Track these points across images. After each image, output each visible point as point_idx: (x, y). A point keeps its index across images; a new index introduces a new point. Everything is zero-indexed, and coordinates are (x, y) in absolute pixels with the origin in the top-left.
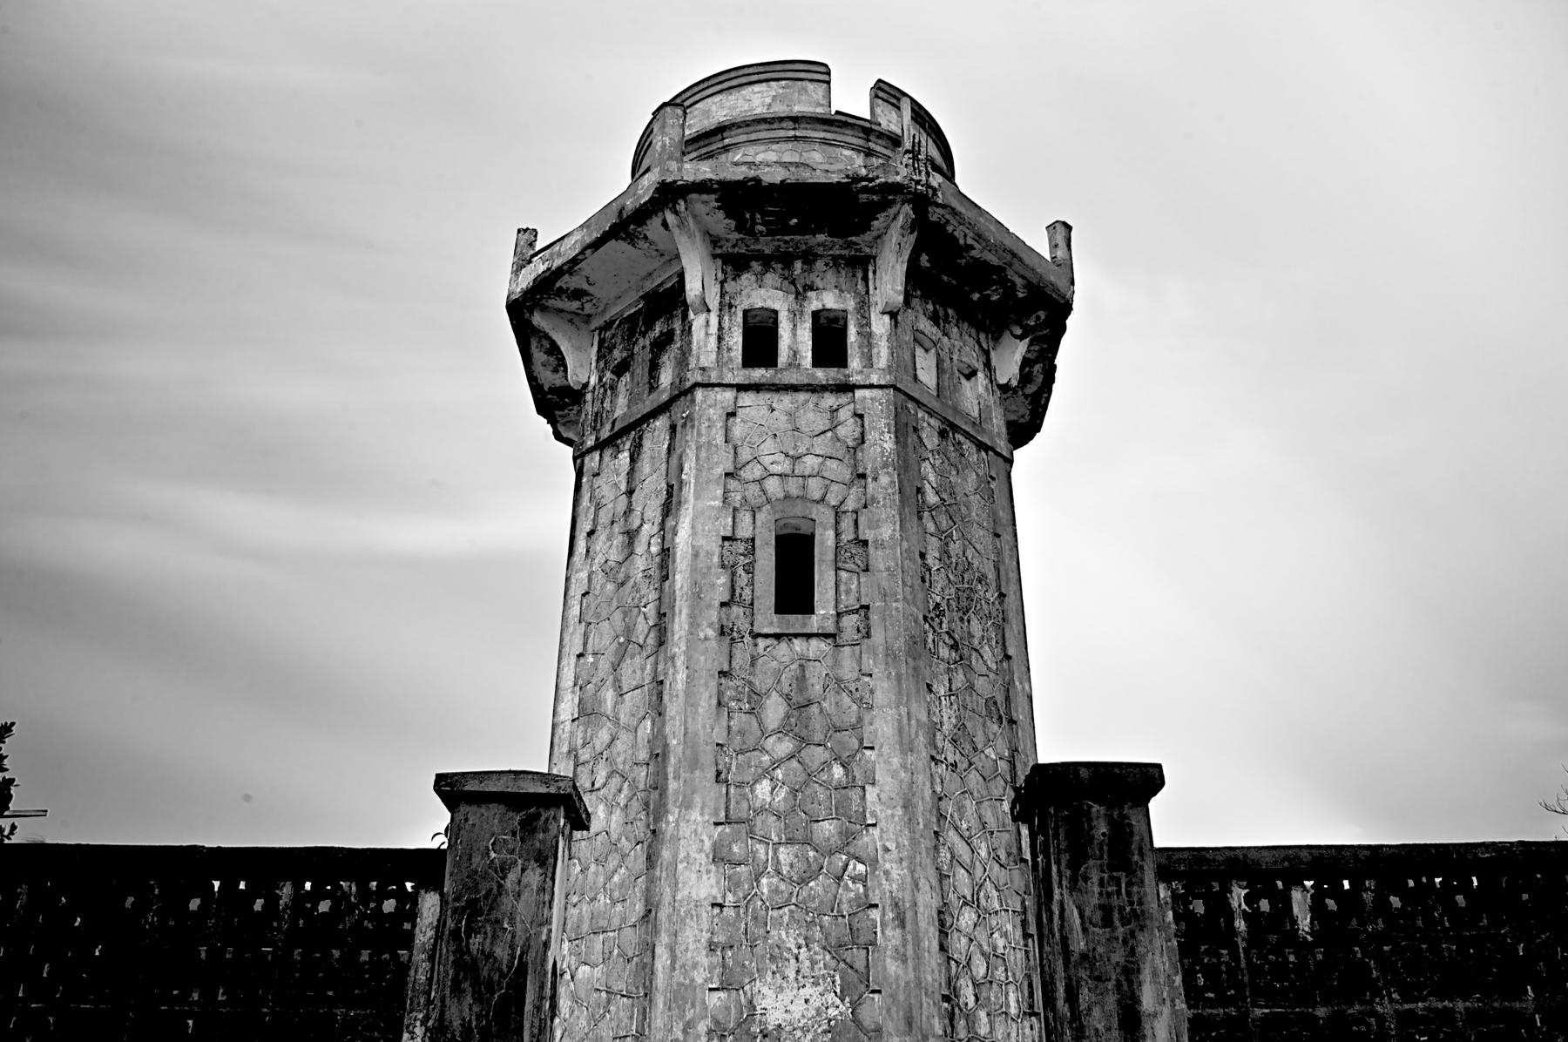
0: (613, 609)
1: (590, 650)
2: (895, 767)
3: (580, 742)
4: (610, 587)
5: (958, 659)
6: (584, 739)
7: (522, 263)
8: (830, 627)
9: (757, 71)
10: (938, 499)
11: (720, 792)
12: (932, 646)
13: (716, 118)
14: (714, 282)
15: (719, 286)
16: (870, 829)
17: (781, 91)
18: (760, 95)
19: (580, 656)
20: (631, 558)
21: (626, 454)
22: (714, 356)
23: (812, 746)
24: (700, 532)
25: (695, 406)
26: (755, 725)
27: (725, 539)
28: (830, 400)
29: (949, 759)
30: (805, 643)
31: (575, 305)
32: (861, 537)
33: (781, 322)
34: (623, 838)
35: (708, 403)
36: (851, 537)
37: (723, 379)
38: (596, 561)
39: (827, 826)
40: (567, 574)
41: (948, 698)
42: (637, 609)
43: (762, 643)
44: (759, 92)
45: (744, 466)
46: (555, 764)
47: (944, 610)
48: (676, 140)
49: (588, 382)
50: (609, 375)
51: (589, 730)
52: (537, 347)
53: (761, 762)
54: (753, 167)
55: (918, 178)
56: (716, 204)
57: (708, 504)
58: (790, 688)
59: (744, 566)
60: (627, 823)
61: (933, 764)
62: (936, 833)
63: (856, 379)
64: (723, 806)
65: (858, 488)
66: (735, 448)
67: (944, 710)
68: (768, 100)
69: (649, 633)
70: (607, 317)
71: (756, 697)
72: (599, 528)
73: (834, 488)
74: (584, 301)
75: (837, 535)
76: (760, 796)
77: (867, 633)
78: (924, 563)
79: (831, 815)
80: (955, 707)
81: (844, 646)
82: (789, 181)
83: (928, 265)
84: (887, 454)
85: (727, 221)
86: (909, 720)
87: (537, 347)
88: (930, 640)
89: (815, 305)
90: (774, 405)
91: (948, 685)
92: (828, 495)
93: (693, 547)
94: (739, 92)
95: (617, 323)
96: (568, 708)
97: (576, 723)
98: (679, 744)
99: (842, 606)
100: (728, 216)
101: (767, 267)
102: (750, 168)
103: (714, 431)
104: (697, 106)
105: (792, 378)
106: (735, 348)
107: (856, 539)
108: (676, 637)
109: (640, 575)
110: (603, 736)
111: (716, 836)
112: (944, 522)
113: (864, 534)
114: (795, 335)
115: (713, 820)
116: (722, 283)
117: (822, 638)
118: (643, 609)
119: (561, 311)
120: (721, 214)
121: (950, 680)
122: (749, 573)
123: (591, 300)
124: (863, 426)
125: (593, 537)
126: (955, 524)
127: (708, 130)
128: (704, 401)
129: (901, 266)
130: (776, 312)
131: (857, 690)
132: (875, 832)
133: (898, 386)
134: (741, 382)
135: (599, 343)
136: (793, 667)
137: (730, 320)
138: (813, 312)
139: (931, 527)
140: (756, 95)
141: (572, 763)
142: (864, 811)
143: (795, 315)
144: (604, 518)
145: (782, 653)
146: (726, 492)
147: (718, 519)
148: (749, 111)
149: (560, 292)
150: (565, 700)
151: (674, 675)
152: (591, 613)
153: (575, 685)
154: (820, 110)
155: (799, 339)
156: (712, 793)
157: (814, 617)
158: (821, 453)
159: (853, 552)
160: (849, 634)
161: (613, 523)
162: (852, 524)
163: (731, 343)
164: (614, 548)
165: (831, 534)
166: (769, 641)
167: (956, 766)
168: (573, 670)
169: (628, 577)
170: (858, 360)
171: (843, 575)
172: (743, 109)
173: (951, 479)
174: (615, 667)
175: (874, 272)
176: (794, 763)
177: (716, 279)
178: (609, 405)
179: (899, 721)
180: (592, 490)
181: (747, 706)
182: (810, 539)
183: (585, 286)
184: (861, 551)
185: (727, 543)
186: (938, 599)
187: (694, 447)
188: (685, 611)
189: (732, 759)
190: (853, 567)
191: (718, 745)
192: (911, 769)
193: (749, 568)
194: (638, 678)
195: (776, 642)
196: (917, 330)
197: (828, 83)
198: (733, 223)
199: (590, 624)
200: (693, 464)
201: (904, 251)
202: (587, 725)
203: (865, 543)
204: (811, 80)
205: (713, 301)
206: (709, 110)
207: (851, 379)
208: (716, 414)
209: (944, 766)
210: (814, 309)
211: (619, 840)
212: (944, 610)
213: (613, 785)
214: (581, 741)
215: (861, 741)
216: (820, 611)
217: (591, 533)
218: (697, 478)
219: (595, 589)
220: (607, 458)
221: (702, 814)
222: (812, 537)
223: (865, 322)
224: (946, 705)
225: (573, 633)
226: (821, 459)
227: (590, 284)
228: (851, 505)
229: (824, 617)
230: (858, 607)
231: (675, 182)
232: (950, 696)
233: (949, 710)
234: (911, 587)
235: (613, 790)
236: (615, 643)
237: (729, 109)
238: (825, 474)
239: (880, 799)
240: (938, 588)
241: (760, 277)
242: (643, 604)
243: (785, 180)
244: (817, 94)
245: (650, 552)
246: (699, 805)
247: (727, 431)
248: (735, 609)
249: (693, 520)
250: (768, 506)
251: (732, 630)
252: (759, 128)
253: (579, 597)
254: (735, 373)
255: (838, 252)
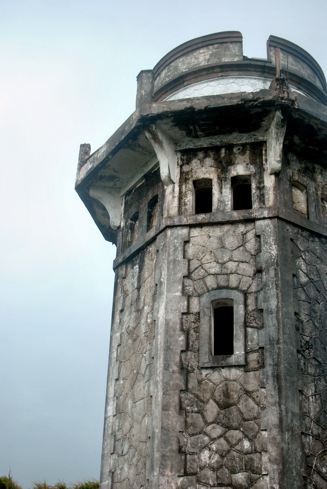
0: (131, 354)
1: (121, 377)
2: (278, 441)
3: (117, 428)
4: (130, 341)
5: (321, 372)
6: (119, 426)
7: (82, 163)
8: (242, 362)
9: (201, 41)
10: (308, 279)
11: (181, 459)
12: (303, 367)
13: (181, 70)
14: (176, 166)
15: (179, 169)
16: (265, 478)
17: (214, 51)
18: (203, 54)
19: (117, 380)
20: (139, 325)
21: (137, 266)
22: (177, 209)
23: (232, 431)
24: (169, 310)
25: (167, 239)
26: (201, 419)
27: (183, 314)
28: (242, 228)
29: (314, 433)
30: (228, 371)
31: (111, 184)
32: (259, 308)
33: (214, 186)
34: (135, 483)
35: (174, 236)
36: (254, 308)
37: (181, 222)
38: (124, 327)
39: (241, 476)
40: (111, 334)
41: (314, 397)
42: (142, 354)
43: (204, 372)
44: (203, 53)
45: (194, 271)
46: (106, 440)
47: (312, 345)
48: (148, 91)
49: (120, 226)
50: (130, 221)
51: (121, 422)
52: (97, 207)
53: (204, 441)
54: (190, 101)
55: (283, 96)
56: (172, 124)
57: (174, 294)
58: (220, 398)
59: (194, 328)
60: (137, 475)
61: (303, 436)
62: (304, 477)
63: (256, 214)
64: (183, 466)
65: (258, 279)
66: (189, 261)
67: (311, 404)
68: (208, 57)
69: (146, 369)
70: (128, 188)
71: (201, 404)
72: (125, 308)
73: (245, 279)
74: (115, 181)
75: (246, 306)
76: (203, 460)
77: (263, 364)
78: (298, 319)
79: (243, 470)
80: (319, 401)
81: (250, 371)
82: (210, 107)
83: (300, 141)
84: (274, 257)
85: (180, 132)
86: (287, 413)
87: (97, 207)
88: (302, 364)
89: (233, 173)
90: (210, 234)
91: (314, 389)
92: (241, 284)
93: (166, 320)
94: (192, 54)
95: (133, 191)
96: (111, 410)
97: (115, 417)
98: (159, 432)
99: (249, 348)
100: (181, 129)
101: (206, 156)
102: (188, 102)
103: (177, 252)
104: (171, 64)
105: (219, 218)
106: (189, 203)
107: (256, 309)
108: (158, 371)
109: (143, 335)
110: (127, 425)
111: (179, 483)
112: (312, 293)
113: (261, 305)
114: (221, 193)
115: (177, 474)
116: (181, 167)
117: (238, 368)
118: (144, 355)
119: (105, 187)
120: (177, 129)
121: (315, 386)
122: (197, 333)
123: (119, 180)
124: (260, 242)
125: (123, 313)
126: (320, 293)
127: (175, 78)
128: (171, 236)
129: (279, 146)
130: (210, 181)
131: (257, 396)
132: (267, 478)
133: (280, 216)
134: (191, 223)
135: (125, 203)
136: (221, 385)
137: (186, 187)
138: (232, 178)
139: (303, 297)
140: (201, 55)
141: (113, 440)
142: (261, 467)
143: (221, 180)
144: (128, 302)
145: (215, 378)
146: (184, 287)
147: (179, 303)
148: (198, 64)
149: (101, 178)
150: (110, 405)
151: (157, 393)
152: (122, 356)
153: (114, 396)
154: (236, 59)
155: (224, 194)
156: (177, 460)
157: (233, 356)
158: (237, 259)
159: (255, 316)
160: (253, 365)
161: (131, 305)
162: (254, 300)
163: (186, 201)
164: (132, 319)
165: (242, 307)
166: (207, 372)
167: (319, 436)
168: (113, 388)
169: (138, 336)
170: (257, 203)
171: (249, 330)
172: (194, 64)
173: (317, 266)
174: (132, 386)
175: (266, 150)
176: (222, 440)
177: (178, 164)
178: (130, 238)
179: (280, 414)
180: (123, 287)
181: (196, 409)
182: (231, 309)
183: (114, 173)
184: (259, 316)
185: (184, 316)
186: (308, 339)
187: (166, 261)
188: (162, 357)
189: (188, 439)
190: (255, 325)
191: (180, 432)
192: (288, 442)
193: (197, 330)
194: (142, 394)
195: (212, 372)
196: (294, 181)
197: (241, 42)
198: (184, 133)
199: (121, 362)
200: (166, 272)
201: (280, 138)
202: (120, 418)
203: (262, 310)
204: (231, 42)
205: (176, 177)
206: (178, 66)
207: (253, 215)
208: (178, 243)
209: (311, 437)
210: (232, 176)
211: (133, 484)
212: (312, 345)
213: (131, 453)
214: (117, 428)
215: (259, 426)
216: (236, 352)
217: (122, 311)
218: (168, 280)
219: (123, 342)
220: (129, 268)
221: (171, 471)
222: (232, 308)
223: (261, 181)
224: (312, 401)
225: (113, 367)
226: (237, 263)
227: (116, 172)
228: (254, 288)
229: (238, 357)
230: (258, 348)
231: (148, 115)
232: (315, 395)
233: (314, 404)
234: (288, 334)
235: (131, 456)
236: (132, 374)
237: (188, 64)
238: (239, 272)
239: (270, 460)
240: (307, 332)
241: (202, 161)
242: (144, 352)
243: (207, 107)
244: (234, 49)
245: (147, 322)
246: (170, 467)
247: (184, 252)
248: (189, 353)
249: (166, 305)
250: (207, 294)
251: (188, 366)
252: (201, 74)
253: (116, 347)
254: (188, 218)
255: (244, 142)
